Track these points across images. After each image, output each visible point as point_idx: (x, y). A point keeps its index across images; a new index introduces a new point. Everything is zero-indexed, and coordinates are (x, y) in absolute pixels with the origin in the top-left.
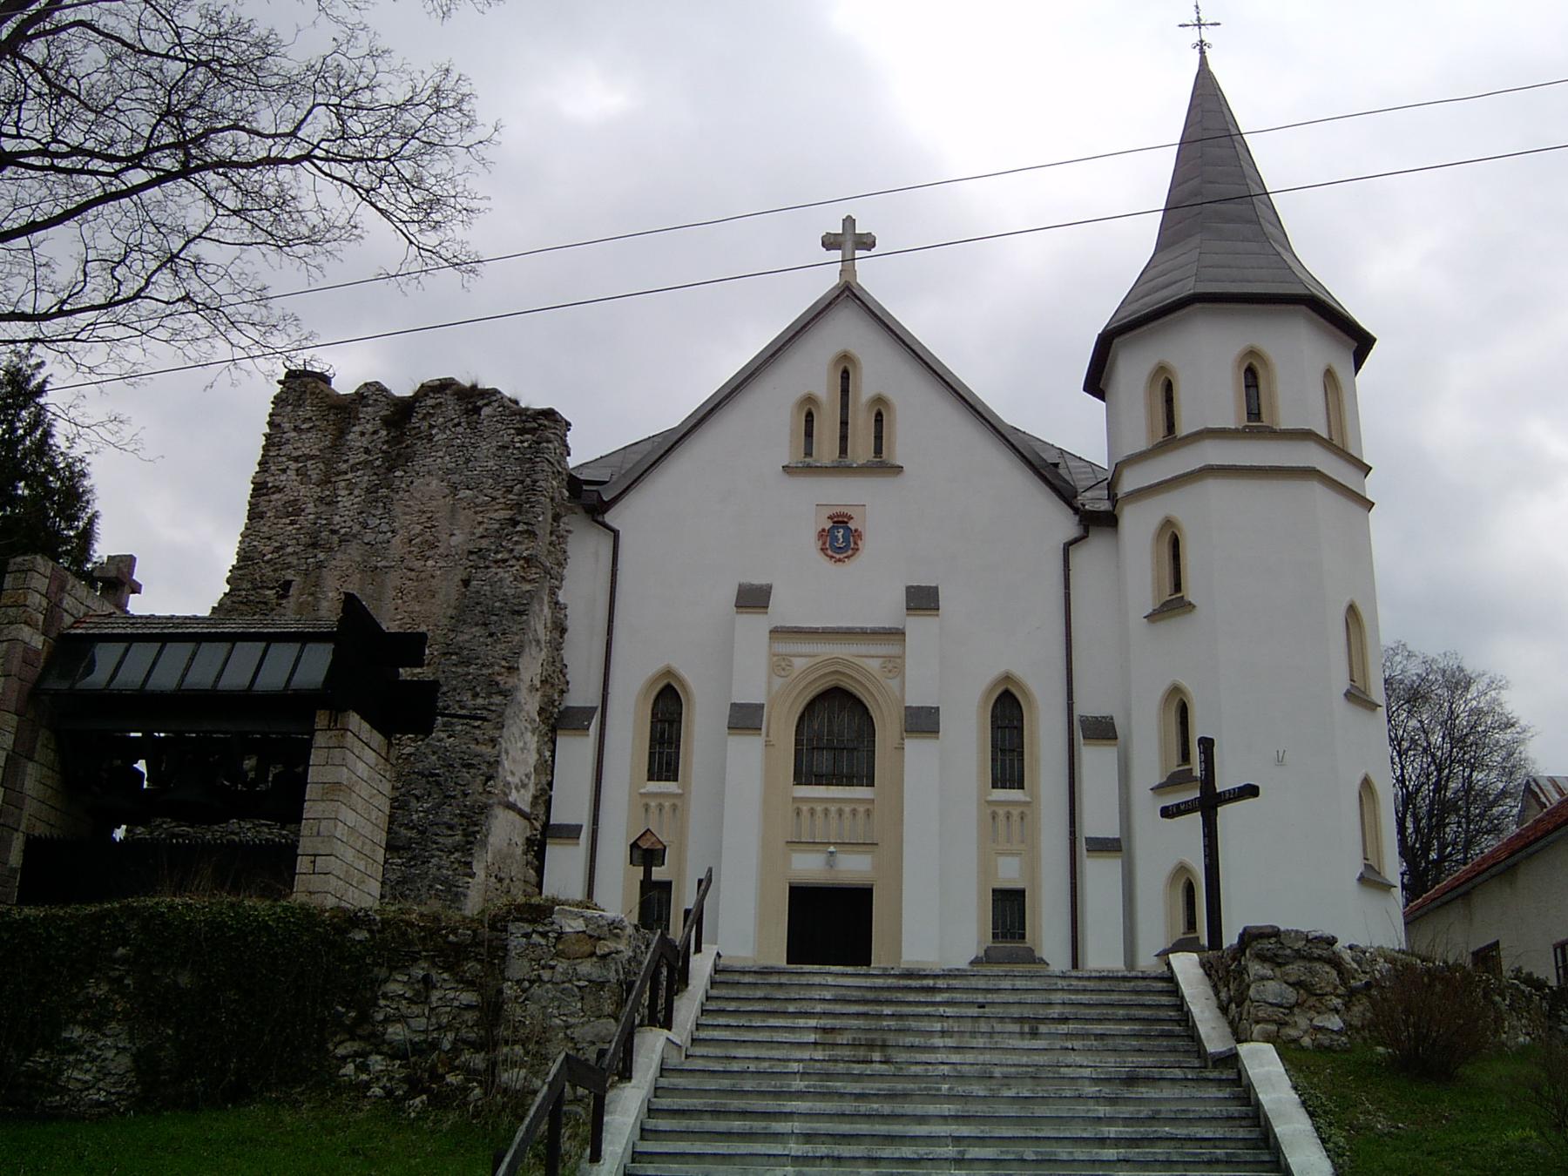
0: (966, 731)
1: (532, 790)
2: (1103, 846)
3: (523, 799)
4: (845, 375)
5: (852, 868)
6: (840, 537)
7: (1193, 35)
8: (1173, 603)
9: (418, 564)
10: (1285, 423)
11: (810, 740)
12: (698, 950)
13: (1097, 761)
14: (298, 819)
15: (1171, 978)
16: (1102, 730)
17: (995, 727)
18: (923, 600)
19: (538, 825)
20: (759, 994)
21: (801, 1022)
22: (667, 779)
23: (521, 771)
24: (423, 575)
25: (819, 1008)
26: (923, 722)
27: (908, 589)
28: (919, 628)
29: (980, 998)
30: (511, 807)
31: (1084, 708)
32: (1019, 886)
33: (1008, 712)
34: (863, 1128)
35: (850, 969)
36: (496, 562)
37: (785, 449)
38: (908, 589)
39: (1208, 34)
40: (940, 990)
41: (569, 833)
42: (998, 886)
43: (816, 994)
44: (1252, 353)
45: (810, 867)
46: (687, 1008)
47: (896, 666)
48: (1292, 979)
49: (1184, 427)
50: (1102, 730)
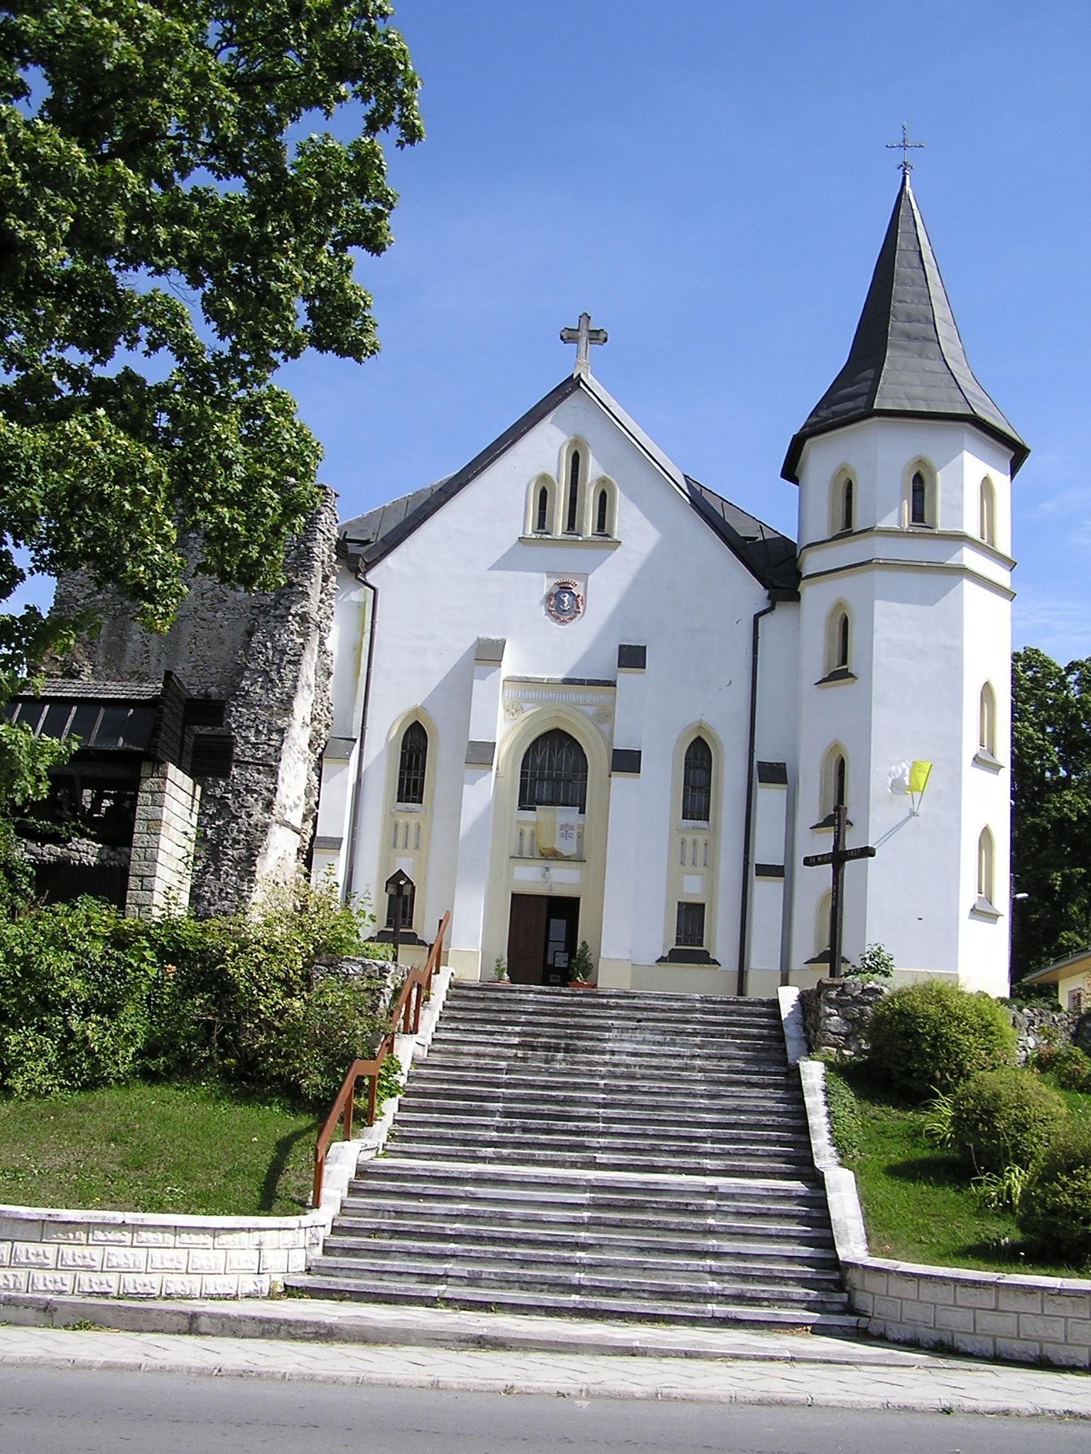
0: (662, 774)
1: (302, 810)
2: (764, 870)
3: (295, 818)
4: (576, 459)
5: (562, 880)
6: (563, 603)
7: (899, 156)
8: (839, 673)
9: (209, 615)
10: (941, 527)
11: (533, 774)
12: (438, 972)
13: (770, 797)
14: (129, 843)
15: (775, 1004)
16: (775, 773)
17: (688, 767)
18: (632, 657)
19: (307, 838)
20: (481, 1005)
21: (510, 1028)
22: (414, 801)
23: (293, 798)
24: (212, 625)
25: (523, 1018)
26: (627, 761)
27: (621, 647)
28: (627, 679)
29: (639, 1015)
30: (286, 824)
31: (761, 755)
32: (700, 901)
33: (699, 757)
34: (545, 1108)
35: (546, 988)
36: (275, 617)
37: (522, 522)
38: (621, 647)
39: (908, 156)
40: (611, 1008)
41: (335, 843)
42: (681, 900)
43: (521, 1007)
44: (921, 462)
45: (531, 879)
46: (429, 1018)
47: (605, 716)
48: (849, 1017)
49: (857, 525)
50: (775, 773)
